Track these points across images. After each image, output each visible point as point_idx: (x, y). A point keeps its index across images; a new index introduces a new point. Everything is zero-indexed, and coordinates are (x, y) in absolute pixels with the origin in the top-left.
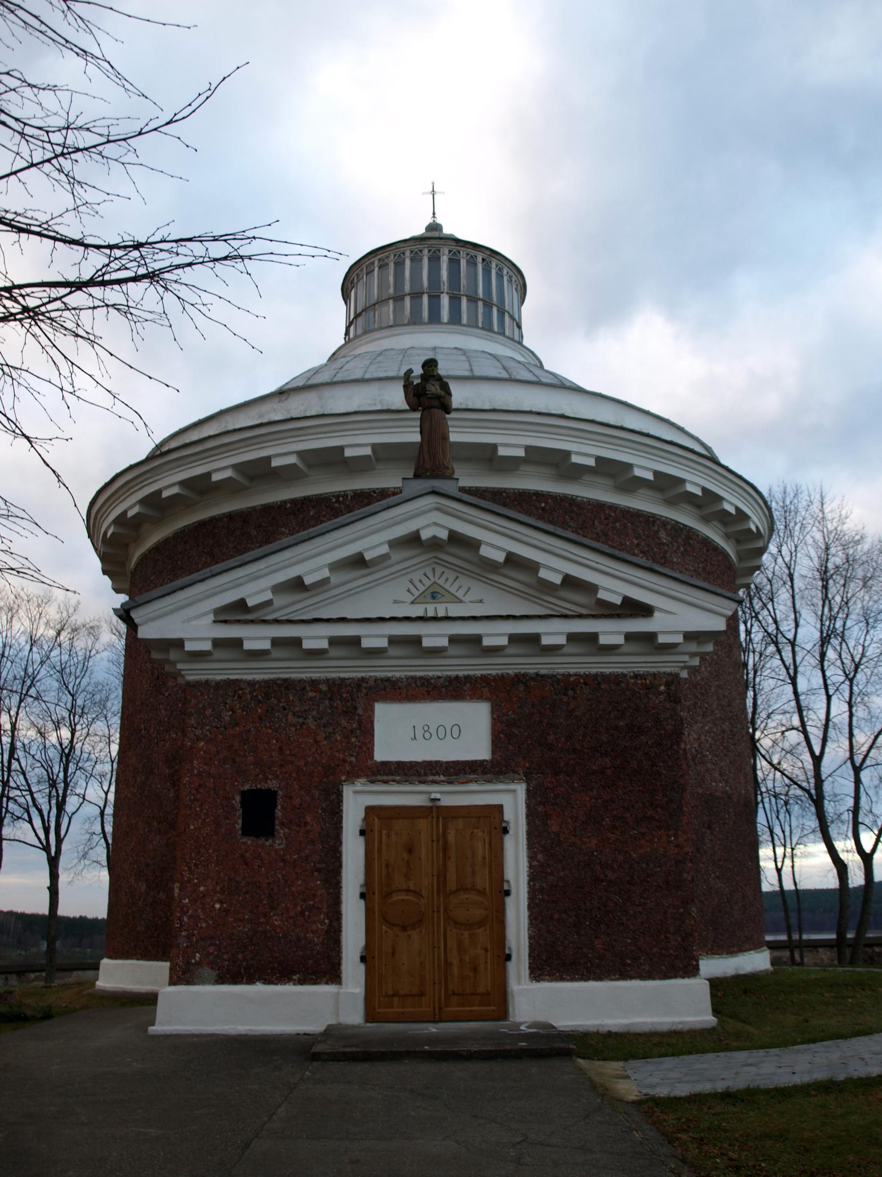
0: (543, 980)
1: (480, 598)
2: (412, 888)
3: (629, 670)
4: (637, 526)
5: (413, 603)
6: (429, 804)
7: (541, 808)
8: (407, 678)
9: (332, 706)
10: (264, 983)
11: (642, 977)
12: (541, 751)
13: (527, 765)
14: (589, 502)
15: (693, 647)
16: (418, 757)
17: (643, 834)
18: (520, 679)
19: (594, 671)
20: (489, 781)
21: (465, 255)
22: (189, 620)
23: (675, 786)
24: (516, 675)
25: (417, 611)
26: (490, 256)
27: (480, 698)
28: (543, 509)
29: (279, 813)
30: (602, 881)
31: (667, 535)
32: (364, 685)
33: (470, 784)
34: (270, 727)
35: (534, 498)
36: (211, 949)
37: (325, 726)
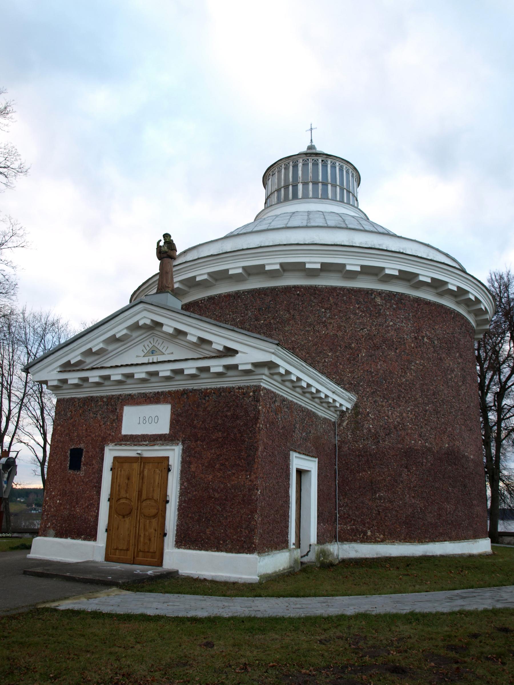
0: (181, 548)
1: (172, 352)
3: (236, 385)
4: (359, 297)
5: (144, 356)
10: (71, 539)
11: (227, 551)
12: (191, 429)
13: (184, 436)
14: (326, 287)
16: (139, 433)
17: (234, 474)
18: (185, 392)
19: (219, 386)
21: (311, 161)
22: (50, 372)
23: (252, 448)
24: (184, 390)
25: (145, 360)
26: (326, 158)
27: (166, 402)
28: (298, 295)
29: (83, 459)
30: (213, 498)
31: (382, 299)
32: (121, 398)
33: (155, 446)
34: (84, 419)
35: (293, 289)
36: (54, 521)
37: (104, 418)
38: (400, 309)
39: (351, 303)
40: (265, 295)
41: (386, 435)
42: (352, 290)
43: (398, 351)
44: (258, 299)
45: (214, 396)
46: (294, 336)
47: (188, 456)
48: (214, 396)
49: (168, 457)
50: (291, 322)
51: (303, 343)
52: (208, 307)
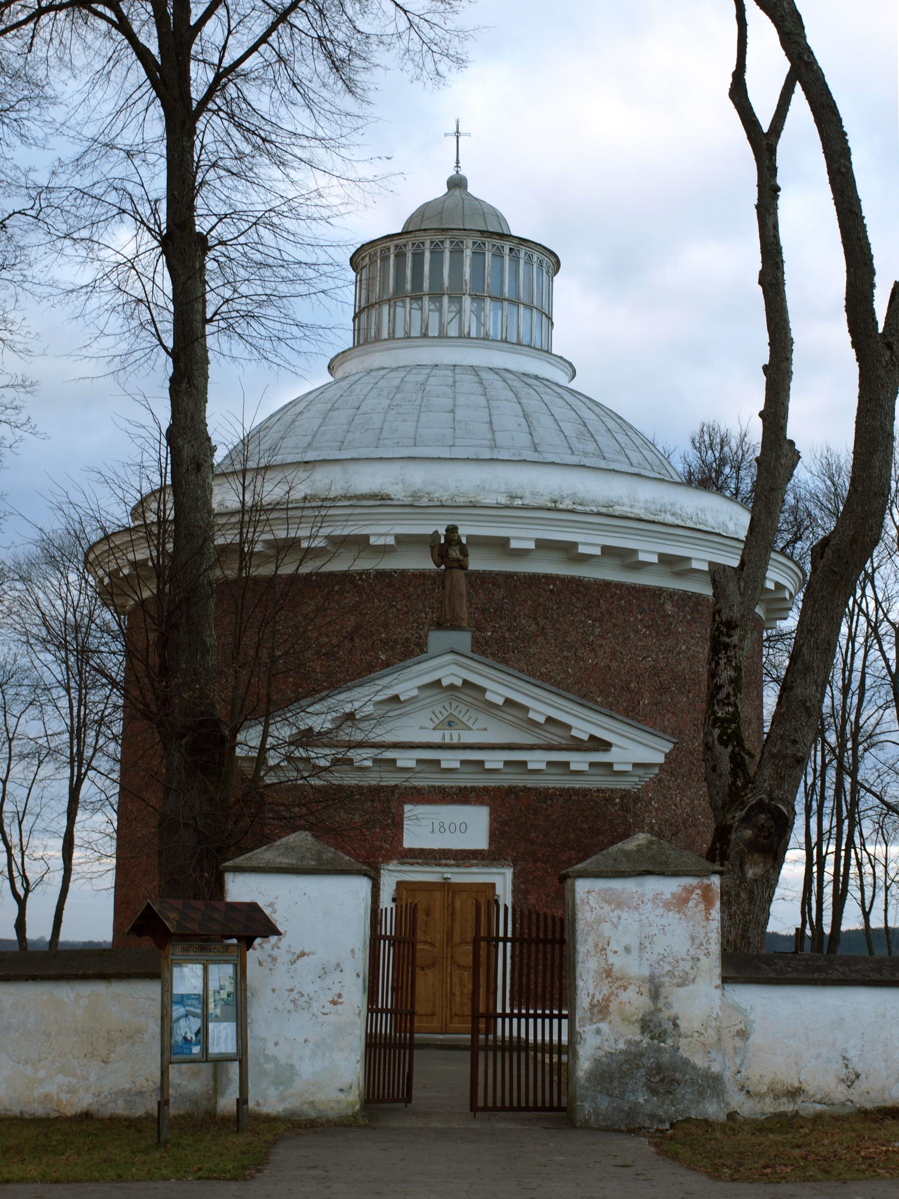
2: (429, 940)
6: (443, 881)
7: (522, 887)
8: (429, 787)
9: (373, 807)
14: (596, 581)
15: (641, 772)
16: (436, 846)
19: (567, 786)
20: (486, 866)
24: (509, 787)
25: (436, 737)
27: (479, 802)
28: (551, 591)
31: (673, 606)
32: (397, 791)
35: (544, 580)
38: (696, 622)
39: (631, 612)
40: (494, 585)
41: (673, 835)
42: (633, 588)
43: (690, 696)
44: (480, 591)
45: (561, 800)
46: (544, 664)
47: (522, 883)
48: (561, 800)
49: (494, 884)
50: (539, 639)
51: (558, 678)
52: (377, 589)
